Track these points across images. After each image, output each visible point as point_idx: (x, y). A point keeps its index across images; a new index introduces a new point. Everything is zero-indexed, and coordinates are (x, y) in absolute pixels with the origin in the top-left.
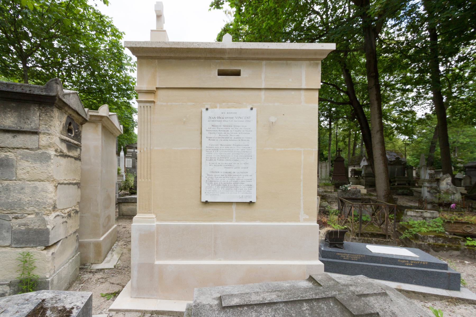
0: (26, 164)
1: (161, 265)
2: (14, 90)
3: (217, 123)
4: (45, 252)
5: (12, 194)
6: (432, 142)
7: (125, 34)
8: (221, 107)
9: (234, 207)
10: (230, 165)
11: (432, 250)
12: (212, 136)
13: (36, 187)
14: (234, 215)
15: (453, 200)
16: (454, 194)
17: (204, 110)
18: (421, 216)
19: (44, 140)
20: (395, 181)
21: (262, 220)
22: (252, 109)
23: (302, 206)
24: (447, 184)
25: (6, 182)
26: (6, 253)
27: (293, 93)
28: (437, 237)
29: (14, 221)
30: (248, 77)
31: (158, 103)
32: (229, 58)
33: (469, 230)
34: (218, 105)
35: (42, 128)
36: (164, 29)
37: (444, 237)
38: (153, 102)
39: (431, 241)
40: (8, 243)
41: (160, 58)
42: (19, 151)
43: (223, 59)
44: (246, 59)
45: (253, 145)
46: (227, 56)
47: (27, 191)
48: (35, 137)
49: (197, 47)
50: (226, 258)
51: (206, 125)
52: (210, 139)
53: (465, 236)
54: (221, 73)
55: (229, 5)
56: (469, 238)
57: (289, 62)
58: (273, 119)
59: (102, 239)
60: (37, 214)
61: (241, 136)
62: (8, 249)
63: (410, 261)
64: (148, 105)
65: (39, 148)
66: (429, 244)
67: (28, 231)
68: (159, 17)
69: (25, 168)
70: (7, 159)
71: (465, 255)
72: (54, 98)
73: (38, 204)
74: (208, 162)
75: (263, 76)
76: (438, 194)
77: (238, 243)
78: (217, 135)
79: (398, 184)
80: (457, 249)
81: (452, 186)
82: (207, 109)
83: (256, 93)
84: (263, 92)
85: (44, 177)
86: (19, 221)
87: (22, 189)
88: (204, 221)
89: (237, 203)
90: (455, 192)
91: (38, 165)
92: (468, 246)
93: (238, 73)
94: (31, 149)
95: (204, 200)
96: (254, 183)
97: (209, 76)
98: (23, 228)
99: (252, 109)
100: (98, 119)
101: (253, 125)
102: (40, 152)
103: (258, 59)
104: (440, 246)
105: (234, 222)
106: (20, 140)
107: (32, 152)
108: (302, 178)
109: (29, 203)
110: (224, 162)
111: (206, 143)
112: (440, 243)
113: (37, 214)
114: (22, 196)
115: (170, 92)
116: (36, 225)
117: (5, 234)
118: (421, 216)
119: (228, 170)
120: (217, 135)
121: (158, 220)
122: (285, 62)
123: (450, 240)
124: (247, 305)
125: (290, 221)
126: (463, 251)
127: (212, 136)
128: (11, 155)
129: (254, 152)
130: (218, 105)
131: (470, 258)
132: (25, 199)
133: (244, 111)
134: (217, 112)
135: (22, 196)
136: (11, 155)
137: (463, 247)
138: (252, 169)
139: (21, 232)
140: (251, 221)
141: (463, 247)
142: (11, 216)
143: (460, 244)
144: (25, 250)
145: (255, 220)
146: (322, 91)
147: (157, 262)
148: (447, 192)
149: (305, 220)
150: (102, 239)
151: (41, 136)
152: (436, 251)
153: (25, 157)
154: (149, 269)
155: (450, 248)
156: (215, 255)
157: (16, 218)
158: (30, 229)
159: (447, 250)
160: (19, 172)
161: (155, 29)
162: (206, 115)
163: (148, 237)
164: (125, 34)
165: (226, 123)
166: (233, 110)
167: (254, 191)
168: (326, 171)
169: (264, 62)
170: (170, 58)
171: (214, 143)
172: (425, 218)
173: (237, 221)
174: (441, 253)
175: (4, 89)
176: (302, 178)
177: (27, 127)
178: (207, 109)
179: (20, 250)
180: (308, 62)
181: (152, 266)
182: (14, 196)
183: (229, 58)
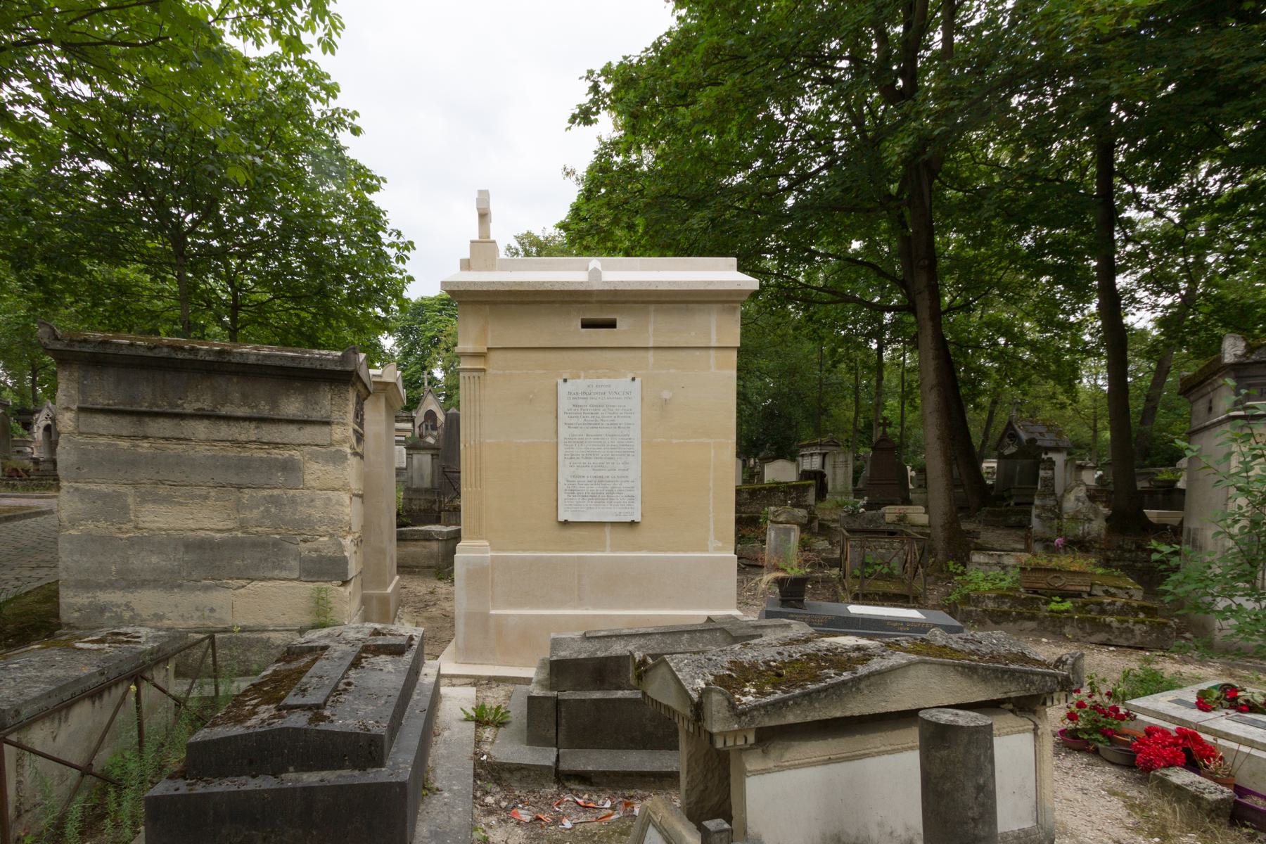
0: (316, 466)
1: (500, 616)
2: (301, 366)
3: (581, 402)
4: (342, 589)
5: (300, 508)
6: (1147, 396)
7: (385, 181)
8: (586, 377)
9: (607, 530)
10: (601, 465)
11: (989, 622)
12: (573, 421)
13: (329, 499)
14: (608, 543)
15: (1089, 534)
16: (1090, 520)
17: (560, 381)
18: (998, 564)
19: (338, 432)
20: (1011, 497)
21: (650, 550)
22: (633, 379)
23: (712, 527)
24: (1078, 499)
25: (292, 492)
26: (293, 588)
27: (698, 353)
28: (1001, 597)
29: (302, 545)
30: (627, 329)
31: (490, 371)
32: (598, 302)
33: (1058, 584)
34: (582, 374)
35: (335, 416)
36: (492, 238)
37: (1014, 598)
38: (483, 370)
39: (991, 605)
40: (296, 575)
41: (494, 303)
42: (307, 448)
43: (589, 303)
44: (624, 302)
45: (636, 434)
46: (594, 299)
47: (318, 503)
48: (326, 429)
49: (550, 288)
50: (595, 607)
51: (564, 404)
52: (569, 425)
53: (1052, 593)
54: (586, 325)
55: (610, 64)
56: (1057, 599)
57: (691, 306)
58: (666, 394)
59: (389, 590)
60: (332, 535)
61: (619, 421)
62: (296, 583)
63: (905, 623)
64: (476, 374)
65: (331, 445)
66: (985, 611)
67: (321, 559)
68: (484, 216)
69: (315, 472)
70: (291, 458)
71: (1045, 629)
72: (349, 374)
73: (332, 522)
74: (568, 462)
75: (651, 329)
76: (1056, 521)
77: (613, 583)
78: (581, 421)
79: (1016, 504)
80: (1032, 618)
81: (1088, 503)
82: (565, 380)
83: (641, 354)
84: (651, 354)
85: (338, 484)
86: (308, 545)
87: (312, 501)
88: (563, 551)
89: (613, 524)
90: (1091, 516)
91: (330, 468)
92: (1052, 611)
93: (611, 325)
94: (322, 446)
95: (561, 519)
96: (637, 493)
97: (570, 330)
98: (314, 555)
99: (633, 379)
100: (381, 387)
101: (635, 404)
102: (333, 449)
103: (643, 302)
104: (1004, 612)
105: (607, 553)
106: (307, 434)
107: (324, 450)
108: (711, 485)
109: (321, 521)
110: (592, 461)
111: (563, 432)
112: (1005, 607)
113: (332, 535)
114: (311, 511)
115: (509, 355)
116: (330, 552)
117: (293, 563)
118: (998, 564)
119: (599, 474)
120: (581, 421)
121: (492, 550)
122: (683, 306)
123: (1023, 602)
124: (616, 636)
125: (693, 551)
126: (1041, 622)
127: (573, 421)
128: (296, 454)
129: (637, 446)
130: (582, 374)
131: (1054, 633)
132: (317, 515)
133: (623, 383)
134: (580, 384)
135: (311, 511)
136: (296, 454)
137: (1041, 615)
138: (635, 470)
139: (312, 560)
140: (633, 550)
141: (1041, 615)
142: (298, 538)
143: (1039, 609)
144: (317, 584)
145: (640, 549)
146: (742, 351)
147: (492, 612)
148: (1075, 518)
149: (717, 549)
150: (389, 590)
151: (334, 427)
152: (996, 623)
153: (314, 458)
154: (482, 621)
155: (1020, 616)
156: (580, 602)
157: (305, 541)
158: (324, 557)
159: (1015, 621)
160: (307, 477)
161: (476, 238)
162: (563, 389)
163: (480, 573)
164: (385, 181)
165: (595, 402)
166: (605, 381)
167: (638, 504)
168: (846, 473)
169: (652, 307)
170: (510, 303)
171: (576, 432)
172: (1004, 567)
173: (612, 551)
174: (1004, 625)
175: (289, 364)
176: (711, 485)
177: (316, 416)
178: (565, 380)
179: (311, 585)
180: (720, 306)
181: (486, 617)
182: (303, 511)
183: (598, 302)
